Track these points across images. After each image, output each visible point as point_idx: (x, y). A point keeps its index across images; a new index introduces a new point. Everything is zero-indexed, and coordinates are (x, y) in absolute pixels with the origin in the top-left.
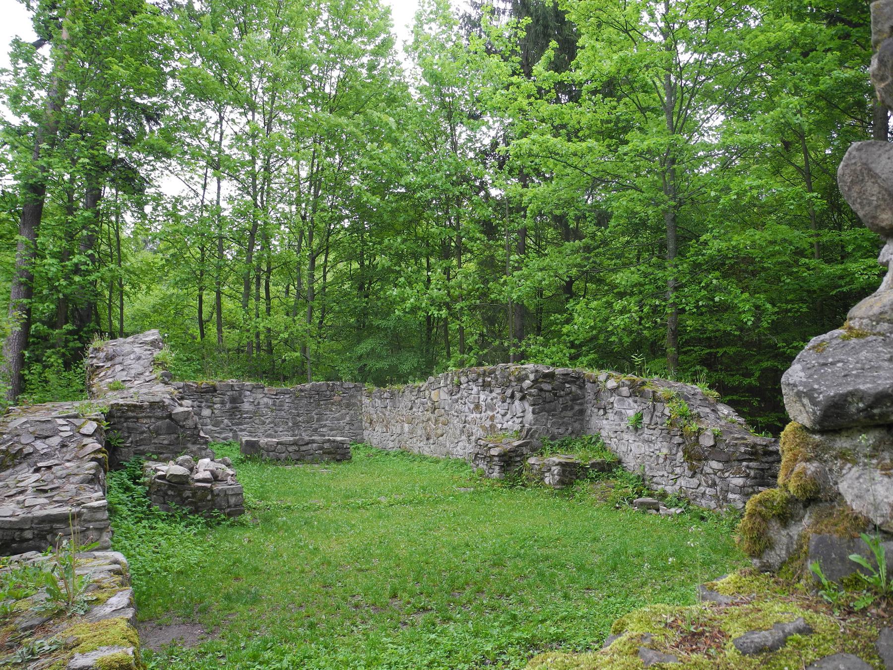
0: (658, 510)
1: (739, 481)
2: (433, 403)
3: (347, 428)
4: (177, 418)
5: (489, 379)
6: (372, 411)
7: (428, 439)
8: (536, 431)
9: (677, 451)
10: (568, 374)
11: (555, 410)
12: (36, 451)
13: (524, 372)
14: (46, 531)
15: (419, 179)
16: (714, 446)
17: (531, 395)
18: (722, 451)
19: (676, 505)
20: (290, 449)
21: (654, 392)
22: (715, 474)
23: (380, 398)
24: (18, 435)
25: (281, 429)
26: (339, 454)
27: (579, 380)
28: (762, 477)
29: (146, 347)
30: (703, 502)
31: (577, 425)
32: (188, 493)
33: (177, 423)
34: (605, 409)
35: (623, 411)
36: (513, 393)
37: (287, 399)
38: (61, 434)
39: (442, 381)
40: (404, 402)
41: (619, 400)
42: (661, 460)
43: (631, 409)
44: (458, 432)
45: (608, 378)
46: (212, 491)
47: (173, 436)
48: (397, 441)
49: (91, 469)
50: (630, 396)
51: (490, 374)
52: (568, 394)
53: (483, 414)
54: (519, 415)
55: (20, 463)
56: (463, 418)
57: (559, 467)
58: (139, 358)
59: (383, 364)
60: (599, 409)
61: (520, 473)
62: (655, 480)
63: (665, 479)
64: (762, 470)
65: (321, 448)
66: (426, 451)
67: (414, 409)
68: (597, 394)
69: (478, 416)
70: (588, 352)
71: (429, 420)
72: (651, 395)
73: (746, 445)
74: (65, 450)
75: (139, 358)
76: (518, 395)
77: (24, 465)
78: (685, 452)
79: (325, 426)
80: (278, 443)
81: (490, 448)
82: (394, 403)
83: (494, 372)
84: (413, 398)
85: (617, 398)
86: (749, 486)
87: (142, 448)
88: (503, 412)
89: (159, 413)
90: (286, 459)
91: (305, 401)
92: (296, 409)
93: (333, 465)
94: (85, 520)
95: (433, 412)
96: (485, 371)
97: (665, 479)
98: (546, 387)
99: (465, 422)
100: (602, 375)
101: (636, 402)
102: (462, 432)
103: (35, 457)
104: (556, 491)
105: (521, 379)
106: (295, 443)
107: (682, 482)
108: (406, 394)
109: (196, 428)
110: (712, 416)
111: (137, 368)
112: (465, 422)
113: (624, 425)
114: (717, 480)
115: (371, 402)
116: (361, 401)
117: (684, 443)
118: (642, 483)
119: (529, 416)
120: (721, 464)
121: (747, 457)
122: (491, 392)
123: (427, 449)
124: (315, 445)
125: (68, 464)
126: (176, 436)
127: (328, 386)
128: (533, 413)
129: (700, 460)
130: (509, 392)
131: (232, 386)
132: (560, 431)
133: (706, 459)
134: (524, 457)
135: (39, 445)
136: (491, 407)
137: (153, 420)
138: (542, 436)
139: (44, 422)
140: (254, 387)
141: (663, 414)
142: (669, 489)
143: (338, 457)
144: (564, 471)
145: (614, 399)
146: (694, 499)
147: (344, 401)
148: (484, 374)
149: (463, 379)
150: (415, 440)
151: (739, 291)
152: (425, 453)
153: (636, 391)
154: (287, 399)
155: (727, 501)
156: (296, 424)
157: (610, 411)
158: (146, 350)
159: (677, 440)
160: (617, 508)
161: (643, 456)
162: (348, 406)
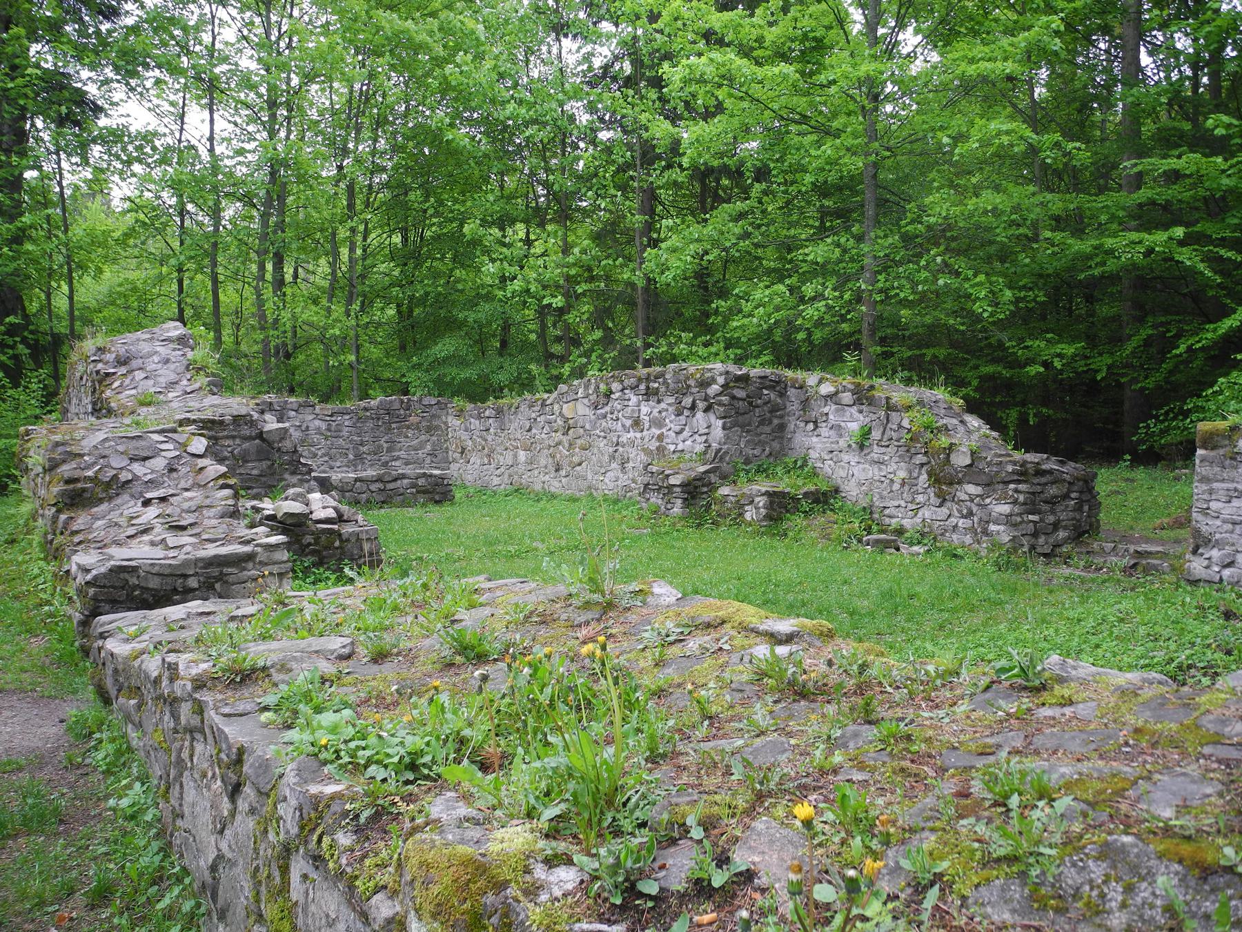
0: (898, 549)
1: (1005, 509)
2: (566, 420)
3: (428, 460)
4: (271, 438)
5: (656, 385)
6: (465, 436)
7: (557, 470)
8: (726, 453)
9: (920, 474)
10: (766, 377)
11: (749, 424)
12: (136, 478)
13: (709, 375)
14: (214, 577)
15: (524, 111)
16: (970, 466)
17: (720, 404)
18: (981, 471)
19: (919, 543)
20: (374, 487)
21: (888, 398)
22: (972, 501)
23: (479, 417)
24: (104, 457)
25: (338, 464)
26: (437, 492)
27: (778, 385)
28: (1033, 503)
29: (171, 346)
30: (955, 537)
31: (776, 445)
32: (309, 539)
33: (270, 444)
34: (815, 422)
35: (843, 424)
36: (694, 402)
37: (346, 420)
38: (163, 453)
39: (581, 391)
40: (517, 424)
41: (837, 411)
42: (896, 486)
43: (854, 421)
44: (606, 458)
45: (820, 382)
46: (340, 535)
47: (265, 464)
48: (506, 476)
49: (227, 498)
51: (657, 377)
52: (765, 404)
53: (645, 433)
54: (702, 431)
55: (118, 495)
56: (615, 440)
57: (765, 498)
58: (167, 361)
59: (469, 373)
60: (807, 422)
61: (709, 506)
62: (887, 512)
63: (902, 510)
64: (1033, 493)
65: (414, 486)
66: (555, 486)
67: (534, 431)
68: (805, 404)
69: (639, 435)
70: (761, 352)
72: (884, 402)
73: (1014, 463)
74: (174, 475)
75: (167, 361)
76: (701, 405)
77: (126, 497)
78: (930, 475)
79: (398, 458)
80: (356, 480)
81: (668, 476)
82: (503, 423)
83: (662, 375)
84: (534, 415)
85: (834, 407)
86: (1017, 515)
87: (396, 454)
88: (678, 428)
89: (246, 431)
90: (368, 501)
91: (370, 424)
92: (359, 435)
93: (431, 507)
94: (260, 562)
96: (649, 375)
97: (902, 510)
98: (741, 394)
99: (617, 444)
100: (812, 379)
101: (861, 412)
102: (612, 458)
103: (137, 488)
104: (763, 529)
105: (704, 384)
106: (379, 479)
107: (926, 513)
108: (522, 413)
109: (296, 451)
110: (961, 429)
111: (167, 374)
112: (617, 444)
113: (845, 439)
114: (975, 509)
115: (461, 424)
116: (446, 423)
117: (929, 462)
118: (870, 517)
119: (718, 432)
120: (980, 488)
121: (1016, 477)
122: (659, 402)
123: (557, 484)
124: (406, 481)
125: (187, 494)
126: (269, 463)
127: (402, 402)
128: (724, 428)
129: (951, 484)
130: (687, 401)
131: (271, 404)
132: (755, 452)
133: (960, 483)
134: (713, 488)
135: (137, 468)
136: (658, 423)
137: (238, 441)
138: (734, 458)
139: (133, 438)
140: (300, 405)
141: (900, 426)
142: (907, 523)
143: (437, 498)
144: (771, 503)
145: (830, 408)
146: (942, 535)
147: (424, 424)
148: (648, 379)
149: (616, 386)
150: (536, 472)
151: (970, 273)
152: (553, 490)
153: (863, 397)
154: (346, 420)
155: (987, 535)
156: (359, 457)
158: (174, 350)
159: (920, 459)
160: (846, 548)
161: (872, 481)
162: (429, 429)
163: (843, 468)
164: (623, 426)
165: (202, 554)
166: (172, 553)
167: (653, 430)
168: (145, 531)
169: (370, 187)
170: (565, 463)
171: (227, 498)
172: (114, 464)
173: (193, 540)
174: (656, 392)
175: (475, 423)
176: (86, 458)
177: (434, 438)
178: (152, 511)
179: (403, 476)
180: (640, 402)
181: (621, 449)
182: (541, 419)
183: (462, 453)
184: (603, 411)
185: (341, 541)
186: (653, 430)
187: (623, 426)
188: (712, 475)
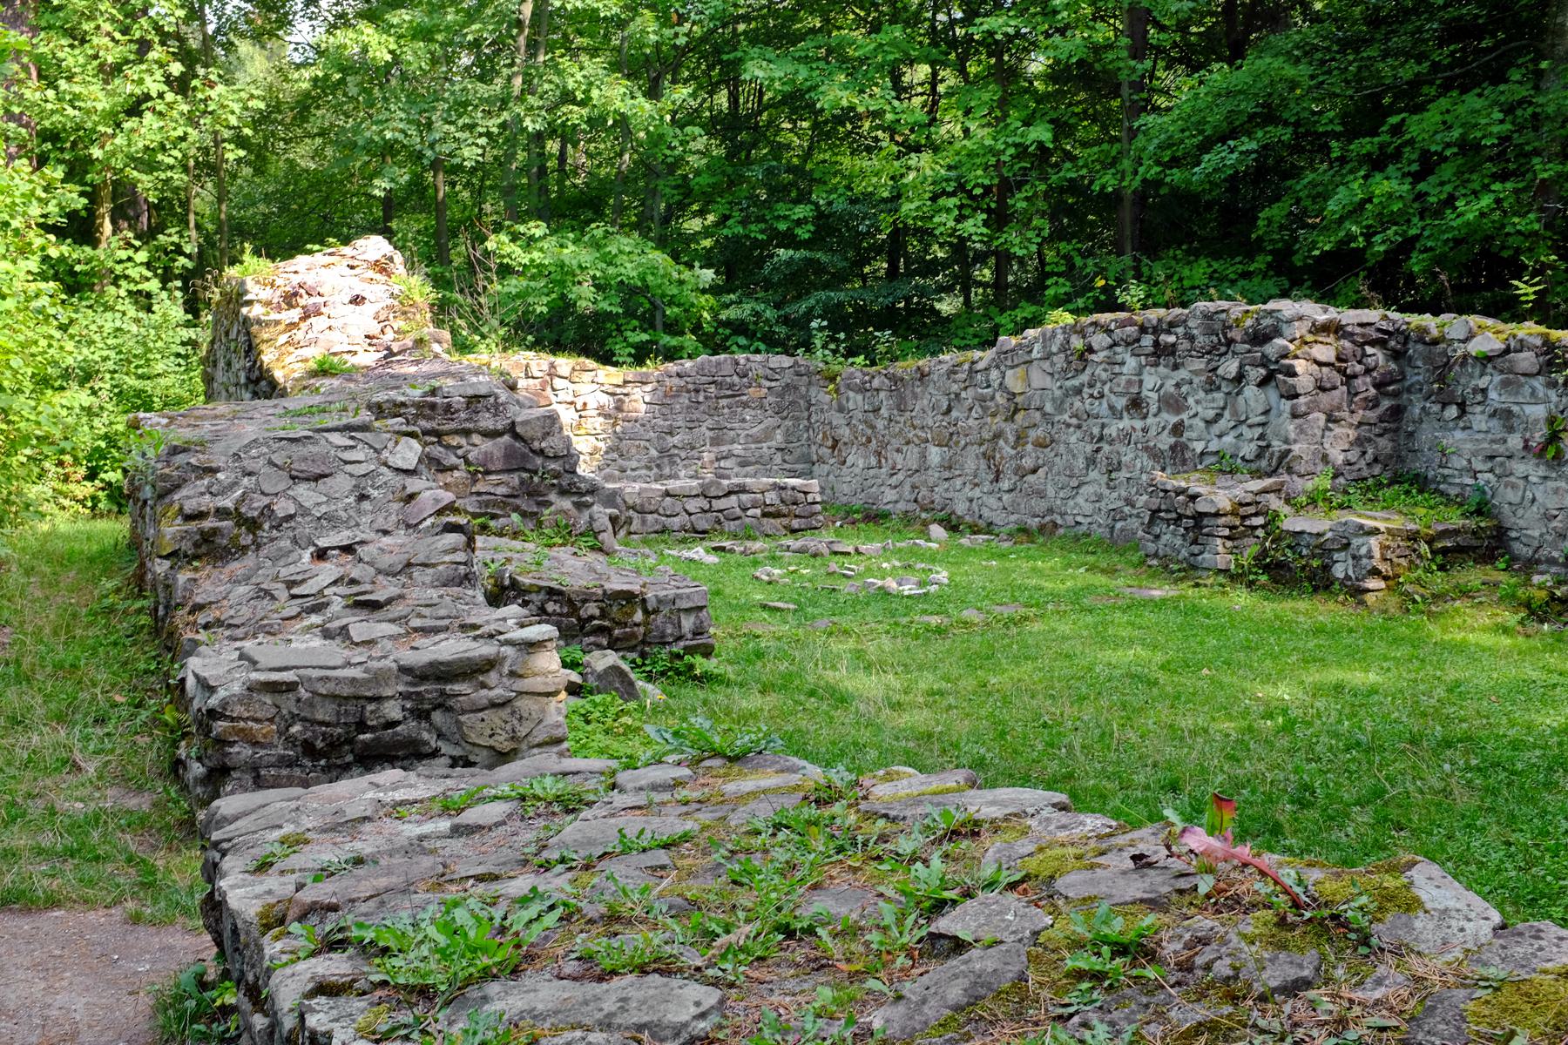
3: (778, 458)
6: (838, 419)
20: (692, 505)
25: (634, 464)
34: (1462, 407)
35: (1515, 408)
38: (348, 468)
39: (1037, 347)
41: (1505, 384)
44: (1080, 463)
48: (907, 487)
50: (1539, 373)
53: (1150, 420)
56: (1096, 431)
60: (1444, 405)
67: (954, 414)
69: (1139, 424)
71: (998, 436)
84: (955, 388)
85: (1498, 378)
88: (1211, 414)
89: (487, 422)
95: (1010, 418)
99: (1101, 439)
102: (1091, 462)
103: (304, 527)
112: (1101, 439)
122: (1176, 367)
123: (992, 501)
130: (1230, 367)
135: (303, 491)
143: (795, 523)
147: (771, 399)
149: (1099, 340)
150: (958, 482)
157: (1479, 409)
163: (1514, 486)
164: (1111, 408)
165: (409, 658)
166: (358, 656)
167: (1165, 415)
168: (317, 609)
169: (574, 690)
170: (1008, 468)
171: (455, 550)
172: (267, 488)
173: (393, 629)
174: (1171, 350)
175: (855, 400)
176: (220, 476)
177: (789, 423)
178: (328, 571)
179: (742, 490)
180: (1141, 367)
181: (1106, 448)
182: (967, 395)
183: (833, 447)
184: (1076, 382)
185: (646, 612)
186: (1165, 415)
187: (1111, 408)
188: (1272, 496)
